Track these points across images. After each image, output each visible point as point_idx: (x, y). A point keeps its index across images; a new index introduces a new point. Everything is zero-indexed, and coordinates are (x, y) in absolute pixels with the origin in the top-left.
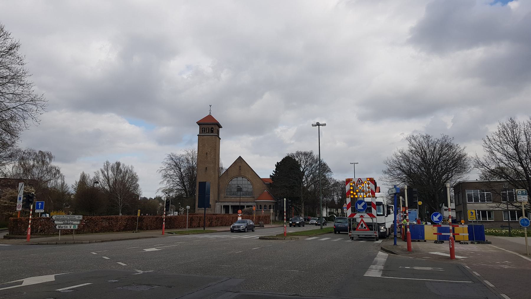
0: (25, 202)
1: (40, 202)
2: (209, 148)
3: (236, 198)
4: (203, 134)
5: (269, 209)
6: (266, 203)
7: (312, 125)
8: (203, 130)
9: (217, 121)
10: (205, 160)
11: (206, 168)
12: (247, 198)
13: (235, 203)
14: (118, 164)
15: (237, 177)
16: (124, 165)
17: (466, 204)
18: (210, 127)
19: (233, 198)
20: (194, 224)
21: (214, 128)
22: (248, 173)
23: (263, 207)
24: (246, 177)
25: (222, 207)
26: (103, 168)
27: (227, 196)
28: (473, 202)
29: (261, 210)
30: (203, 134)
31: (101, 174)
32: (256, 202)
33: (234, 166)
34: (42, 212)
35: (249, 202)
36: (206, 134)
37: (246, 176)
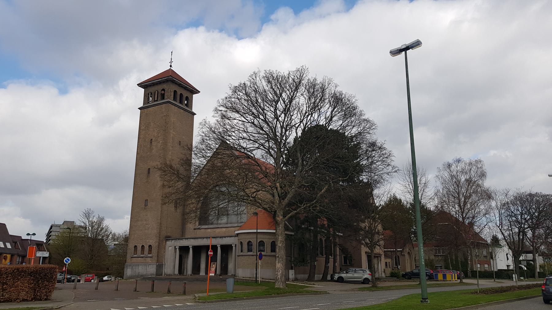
3: (215, 229)
5: (272, 251)
6: (251, 236)
7: (549, 175)
10: (148, 153)
12: (224, 229)
13: (200, 240)
19: (209, 230)
20: (317, 277)
25: (178, 249)
34: (44, 256)
35: (225, 237)
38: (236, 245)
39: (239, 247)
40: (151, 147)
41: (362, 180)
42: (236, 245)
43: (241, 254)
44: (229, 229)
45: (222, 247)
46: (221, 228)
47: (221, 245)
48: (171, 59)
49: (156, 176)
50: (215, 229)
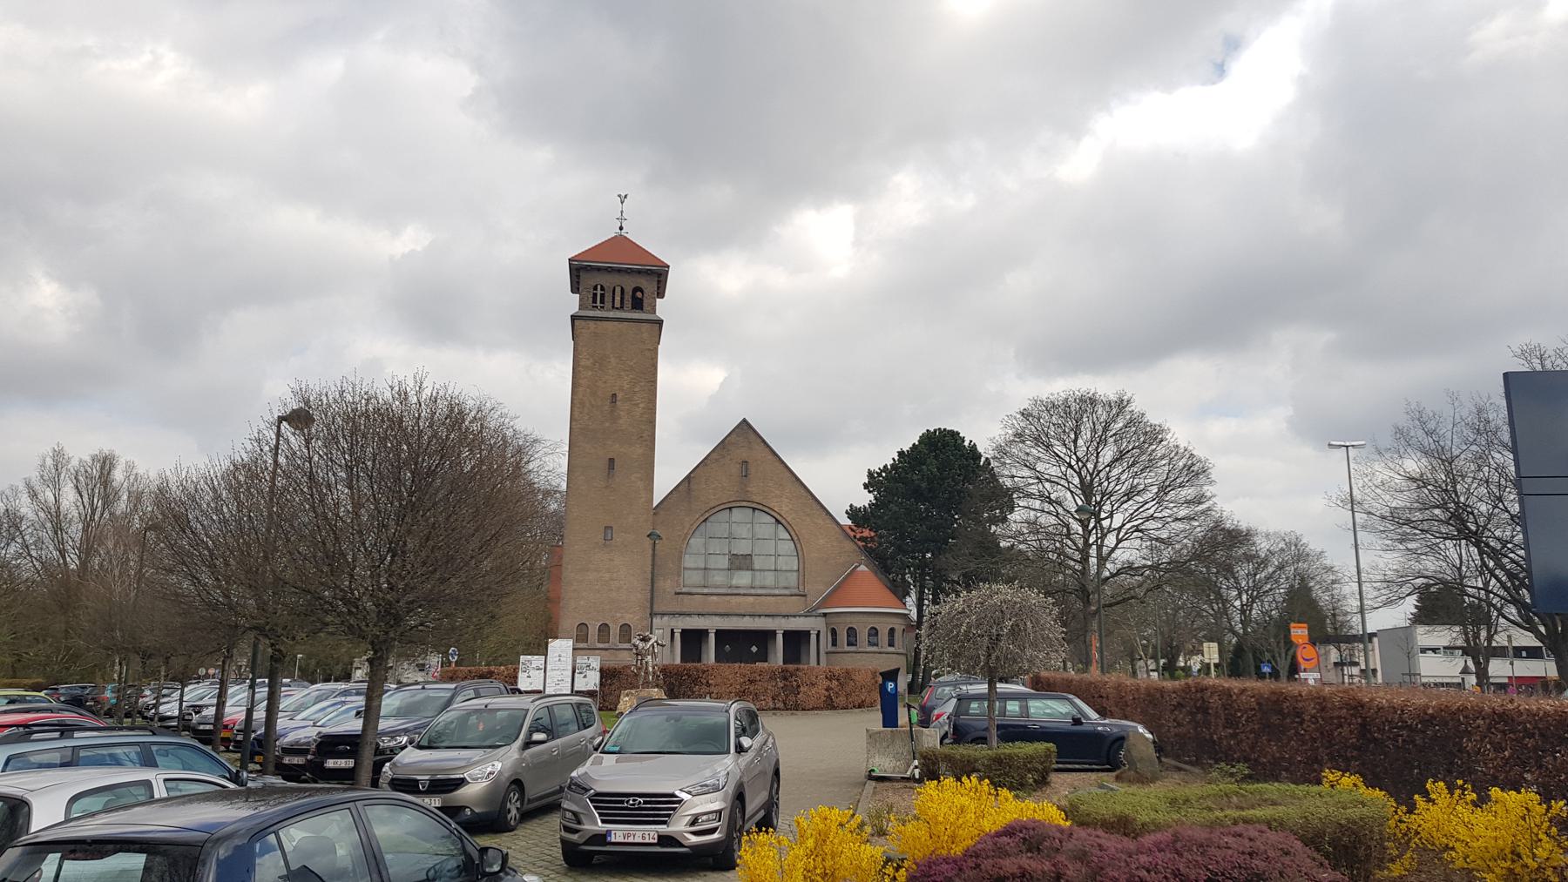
0: (1486, 644)
1: (913, 770)
2: (622, 373)
4: (598, 313)
6: (877, 619)
8: (595, 295)
9: (663, 262)
11: (612, 460)
12: (751, 598)
13: (735, 619)
14: (106, 464)
15: (730, 508)
16: (130, 467)
18: (629, 283)
19: (715, 598)
23: (863, 636)
25: (678, 636)
26: (34, 476)
27: (684, 590)
29: (852, 649)
30: (598, 313)
31: (25, 498)
32: (825, 615)
33: (717, 460)
35: (795, 616)
36: (612, 314)
38: (819, 631)
39: (825, 640)
43: (834, 649)
44: (763, 598)
45: (786, 634)
46: (744, 595)
48: (622, 212)
49: (633, 479)
50: (729, 597)
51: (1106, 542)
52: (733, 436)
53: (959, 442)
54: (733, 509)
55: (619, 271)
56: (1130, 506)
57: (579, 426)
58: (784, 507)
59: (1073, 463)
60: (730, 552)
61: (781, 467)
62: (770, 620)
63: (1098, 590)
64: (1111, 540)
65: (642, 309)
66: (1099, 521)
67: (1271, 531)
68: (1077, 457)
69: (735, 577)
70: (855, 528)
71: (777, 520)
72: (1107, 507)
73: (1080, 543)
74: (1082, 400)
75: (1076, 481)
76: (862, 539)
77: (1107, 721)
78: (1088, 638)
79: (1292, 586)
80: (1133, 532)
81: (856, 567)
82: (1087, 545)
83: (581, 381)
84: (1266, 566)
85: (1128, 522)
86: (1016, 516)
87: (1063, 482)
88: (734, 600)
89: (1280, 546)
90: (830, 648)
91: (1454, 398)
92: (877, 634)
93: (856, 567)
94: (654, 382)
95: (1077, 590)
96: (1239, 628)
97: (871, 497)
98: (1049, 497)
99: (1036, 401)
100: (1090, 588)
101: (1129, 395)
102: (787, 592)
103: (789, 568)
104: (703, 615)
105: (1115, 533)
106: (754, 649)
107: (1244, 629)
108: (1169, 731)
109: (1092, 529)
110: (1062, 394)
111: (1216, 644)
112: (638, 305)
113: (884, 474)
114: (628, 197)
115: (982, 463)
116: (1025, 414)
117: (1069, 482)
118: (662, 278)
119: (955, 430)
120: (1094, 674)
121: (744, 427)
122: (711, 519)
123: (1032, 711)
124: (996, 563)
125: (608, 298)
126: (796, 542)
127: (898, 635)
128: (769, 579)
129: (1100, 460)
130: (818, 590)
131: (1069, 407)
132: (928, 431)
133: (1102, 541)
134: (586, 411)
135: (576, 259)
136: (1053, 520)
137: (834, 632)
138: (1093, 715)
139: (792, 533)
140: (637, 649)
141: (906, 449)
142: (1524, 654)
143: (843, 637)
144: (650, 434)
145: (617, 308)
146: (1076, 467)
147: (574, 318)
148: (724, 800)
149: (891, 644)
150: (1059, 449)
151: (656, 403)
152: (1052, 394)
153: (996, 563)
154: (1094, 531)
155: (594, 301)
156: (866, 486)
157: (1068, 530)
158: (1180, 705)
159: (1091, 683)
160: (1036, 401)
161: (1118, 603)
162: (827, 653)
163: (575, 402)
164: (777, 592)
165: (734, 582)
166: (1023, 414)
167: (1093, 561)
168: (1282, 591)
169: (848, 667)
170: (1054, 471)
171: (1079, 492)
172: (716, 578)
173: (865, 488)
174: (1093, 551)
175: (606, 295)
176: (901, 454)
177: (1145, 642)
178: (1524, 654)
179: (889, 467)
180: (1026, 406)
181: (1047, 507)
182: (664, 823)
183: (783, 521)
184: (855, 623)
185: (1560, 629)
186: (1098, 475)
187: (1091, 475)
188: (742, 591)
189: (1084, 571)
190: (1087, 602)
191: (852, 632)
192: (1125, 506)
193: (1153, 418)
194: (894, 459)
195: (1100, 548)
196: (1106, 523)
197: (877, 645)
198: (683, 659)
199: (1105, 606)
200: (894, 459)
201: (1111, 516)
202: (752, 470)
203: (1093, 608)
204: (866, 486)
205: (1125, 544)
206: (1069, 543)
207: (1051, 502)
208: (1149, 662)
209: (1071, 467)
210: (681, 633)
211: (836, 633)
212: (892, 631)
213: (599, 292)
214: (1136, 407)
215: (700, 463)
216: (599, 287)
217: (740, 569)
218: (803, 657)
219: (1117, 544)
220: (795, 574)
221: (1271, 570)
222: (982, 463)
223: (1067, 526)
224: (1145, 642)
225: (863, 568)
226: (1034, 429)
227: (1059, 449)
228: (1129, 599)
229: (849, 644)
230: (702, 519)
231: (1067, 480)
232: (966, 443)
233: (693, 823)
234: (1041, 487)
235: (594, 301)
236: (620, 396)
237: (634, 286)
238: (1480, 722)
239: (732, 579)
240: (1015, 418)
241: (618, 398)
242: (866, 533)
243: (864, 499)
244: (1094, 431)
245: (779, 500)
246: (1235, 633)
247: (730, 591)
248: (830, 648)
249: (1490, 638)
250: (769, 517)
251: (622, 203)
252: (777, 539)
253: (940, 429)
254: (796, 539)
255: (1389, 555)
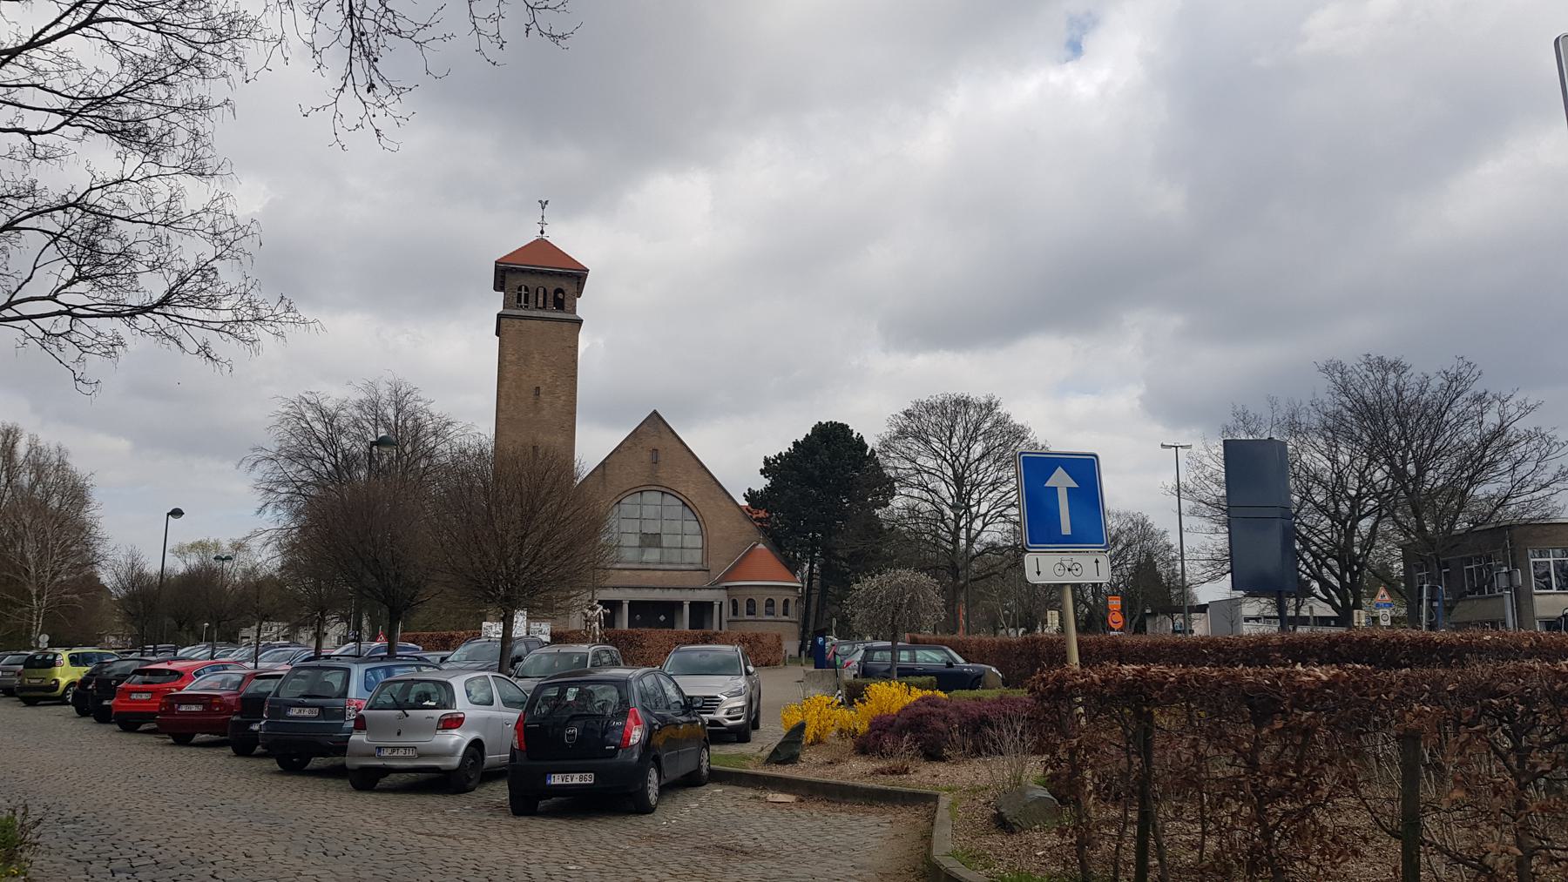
2: (545, 368)
3: (639, 572)
4: (522, 312)
6: (774, 591)
8: (520, 295)
9: (583, 266)
10: (531, 415)
12: (660, 573)
13: (646, 591)
15: (641, 492)
17: (1531, 595)
19: (627, 572)
21: (566, 293)
22: (685, 478)
23: (761, 607)
24: (675, 494)
28: (1554, 590)
30: (522, 312)
32: (727, 588)
33: (630, 448)
35: (700, 589)
36: (535, 314)
37: (679, 490)
38: (721, 603)
40: (536, 403)
41: (878, 515)
42: (721, 603)
43: (734, 618)
44: (670, 572)
45: (692, 604)
47: (630, 601)
51: (974, 525)
52: (645, 426)
53: (849, 434)
54: (644, 493)
55: (542, 273)
56: (995, 495)
57: (505, 416)
58: (691, 492)
59: (948, 457)
60: (641, 531)
61: (688, 454)
62: (678, 592)
63: (967, 566)
64: (978, 524)
65: (563, 309)
66: (968, 507)
67: (1122, 512)
68: (951, 452)
69: (646, 554)
70: (752, 510)
71: (684, 503)
72: (975, 496)
73: (952, 527)
74: (957, 402)
75: (950, 472)
76: (757, 519)
77: (970, 665)
78: (956, 608)
79: (1138, 562)
80: (996, 517)
81: (754, 545)
82: (958, 528)
83: (507, 375)
84: (1116, 544)
85: (993, 509)
86: (898, 502)
87: (938, 473)
88: (645, 574)
89: (1129, 525)
90: (731, 617)
91: (1273, 402)
92: (773, 605)
93: (754, 545)
94: (575, 376)
95: (948, 567)
96: (1090, 599)
97: (767, 482)
98: (927, 487)
99: (918, 403)
100: (959, 565)
101: (997, 398)
102: (692, 567)
103: (694, 546)
104: (617, 588)
105: (981, 518)
106: (662, 618)
107: (1095, 601)
108: (1013, 673)
109: (963, 515)
110: (940, 397)
111: (1057, 612)
112: (560, 305)
113: (779, 461)
114: (549, 203)
115: (868, 453)
116: (908, 414)
117: (944, 474)
118: (581, 281)
119: (845, 423)
120: (960, 635)
121: (655, 414)
122: (623, 501)
123: (918, 657)
124: (880, 543)
125: (532, 298)
126: (701, 522)
127: (791, 606)
128: (675, 556)
129: (971, 456)
130: (720, 566)
131: (946, 409)
132: (819, 423)
133: (971, 525)
134: (512, 402)
135: (502, 261)
136: (928, 506)
137: (735, 603)
138: (961, 660)
139: (698, 515)
140: (586, 616)
141: (800, 439)
142: (1333, 623)
143: (743, 607)
144: (570, 424)
145: (540, 308)
146: (950, 461)
147: (500, 316)
148: (746, 700)
149: (785, 614)
150: (936, 445)
151: (576, 396)
152: (932, 397)
153: (880, 543)
154: (964, 516)
155: (519, 301)
156: (762, 472)
157: (943, 516)
158: (1021, 653)
159: (959, 641)
160: (918, 403)
161: (982, 578)
162: (728, 621)
163: (502, 394)
164: (683, 567)
165: (644, 558)
166: (906, 414)
167: (963, 542)
168: (1128, 566)
169: (758, 632)
170: (931, 464)
171: (952, 483)
172: (628, 554)
173: (761, 474)
174: (963, 534)
175: (530, 295)
176: (796, 444)
177: (1006, 612)
178: (1333, 623)
179: (784, 454)
180: (909, 408)
181: (925, 495)
182: (711, 713)
183: (689, 504)
184: (754, 595)
185: (1351, 602)
186: (969, 467)
187: (963, 468)
188: (652, 567)
189: (954, 551)
190: (956, 578)
191: (751, 603)
192: (990, 495)
193: (1017, 419)
194: (789, 449)
195: (968, 531)
196: (974, 510)
197: (773, 614)
198: (629, 627)
199: (971, 580)
200: (789, 449)
201: (979, 503)
202: (661, 457)
203: (962, 582)
204: (762, 472)
205: (990, 527)
206: (943, 526)
207: (928, 491)
208: (1010, 631)
209: (947, 461)
210: (690, 605)
211: (737, 603)
212: (786, 602)
213: (523, 292)
214: (1002, 409)
215: (615, 450)
216: (523, 287)
217: (649, 547)
218: (707, 624)
219: (983, 528)
220: (700, 551)
221: (1120, 547)
222: (868, 453)
223: (942, 512)
224: (1006, 612)
225: (761, 546)
226: (915, 428)
227: (936, 445)
228: (991, 574)
229: (749, 613)
230: (616, 501)
231: (942, 472)
232: (854, 436)
233: (728, 713)
234: (920, 478)
235: (519, 301)
236: (542, 389)
237: (555, 288)
238: (1167, 650)
239: (643, 555)
240: (899, 417)
241: (541, 391)
242: (762, 514)
243: (761, 483)
244: (966, 429)
245: (686, 484)
246: (1087, 605)
247: (641, 566)
248: (731, 617)
249: (1298, 609)
250: (676, 499)
251: (543, 208)
252: (684, 519)
253: (831, 422)
254: (700, 519)
255: (1217, 537)
